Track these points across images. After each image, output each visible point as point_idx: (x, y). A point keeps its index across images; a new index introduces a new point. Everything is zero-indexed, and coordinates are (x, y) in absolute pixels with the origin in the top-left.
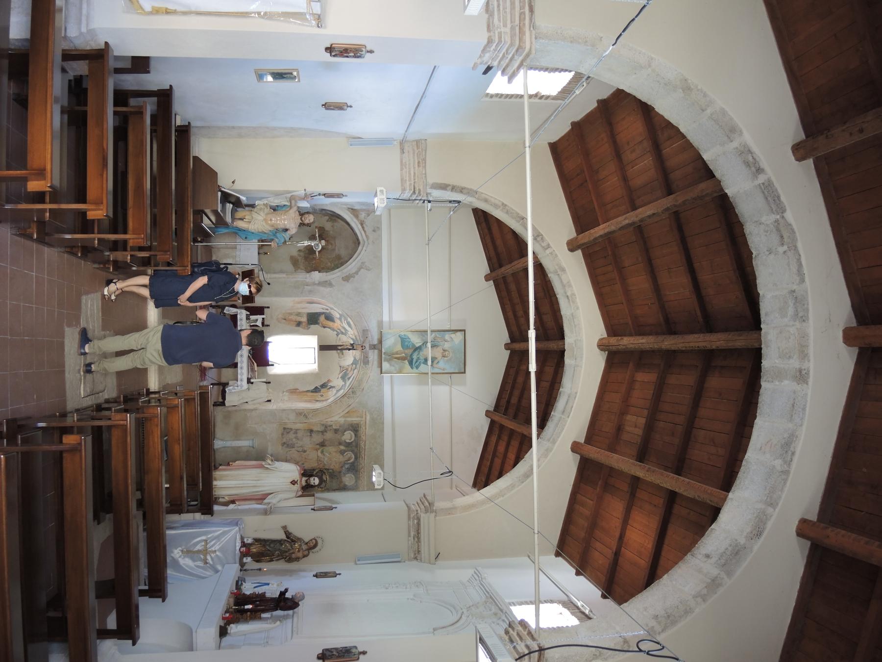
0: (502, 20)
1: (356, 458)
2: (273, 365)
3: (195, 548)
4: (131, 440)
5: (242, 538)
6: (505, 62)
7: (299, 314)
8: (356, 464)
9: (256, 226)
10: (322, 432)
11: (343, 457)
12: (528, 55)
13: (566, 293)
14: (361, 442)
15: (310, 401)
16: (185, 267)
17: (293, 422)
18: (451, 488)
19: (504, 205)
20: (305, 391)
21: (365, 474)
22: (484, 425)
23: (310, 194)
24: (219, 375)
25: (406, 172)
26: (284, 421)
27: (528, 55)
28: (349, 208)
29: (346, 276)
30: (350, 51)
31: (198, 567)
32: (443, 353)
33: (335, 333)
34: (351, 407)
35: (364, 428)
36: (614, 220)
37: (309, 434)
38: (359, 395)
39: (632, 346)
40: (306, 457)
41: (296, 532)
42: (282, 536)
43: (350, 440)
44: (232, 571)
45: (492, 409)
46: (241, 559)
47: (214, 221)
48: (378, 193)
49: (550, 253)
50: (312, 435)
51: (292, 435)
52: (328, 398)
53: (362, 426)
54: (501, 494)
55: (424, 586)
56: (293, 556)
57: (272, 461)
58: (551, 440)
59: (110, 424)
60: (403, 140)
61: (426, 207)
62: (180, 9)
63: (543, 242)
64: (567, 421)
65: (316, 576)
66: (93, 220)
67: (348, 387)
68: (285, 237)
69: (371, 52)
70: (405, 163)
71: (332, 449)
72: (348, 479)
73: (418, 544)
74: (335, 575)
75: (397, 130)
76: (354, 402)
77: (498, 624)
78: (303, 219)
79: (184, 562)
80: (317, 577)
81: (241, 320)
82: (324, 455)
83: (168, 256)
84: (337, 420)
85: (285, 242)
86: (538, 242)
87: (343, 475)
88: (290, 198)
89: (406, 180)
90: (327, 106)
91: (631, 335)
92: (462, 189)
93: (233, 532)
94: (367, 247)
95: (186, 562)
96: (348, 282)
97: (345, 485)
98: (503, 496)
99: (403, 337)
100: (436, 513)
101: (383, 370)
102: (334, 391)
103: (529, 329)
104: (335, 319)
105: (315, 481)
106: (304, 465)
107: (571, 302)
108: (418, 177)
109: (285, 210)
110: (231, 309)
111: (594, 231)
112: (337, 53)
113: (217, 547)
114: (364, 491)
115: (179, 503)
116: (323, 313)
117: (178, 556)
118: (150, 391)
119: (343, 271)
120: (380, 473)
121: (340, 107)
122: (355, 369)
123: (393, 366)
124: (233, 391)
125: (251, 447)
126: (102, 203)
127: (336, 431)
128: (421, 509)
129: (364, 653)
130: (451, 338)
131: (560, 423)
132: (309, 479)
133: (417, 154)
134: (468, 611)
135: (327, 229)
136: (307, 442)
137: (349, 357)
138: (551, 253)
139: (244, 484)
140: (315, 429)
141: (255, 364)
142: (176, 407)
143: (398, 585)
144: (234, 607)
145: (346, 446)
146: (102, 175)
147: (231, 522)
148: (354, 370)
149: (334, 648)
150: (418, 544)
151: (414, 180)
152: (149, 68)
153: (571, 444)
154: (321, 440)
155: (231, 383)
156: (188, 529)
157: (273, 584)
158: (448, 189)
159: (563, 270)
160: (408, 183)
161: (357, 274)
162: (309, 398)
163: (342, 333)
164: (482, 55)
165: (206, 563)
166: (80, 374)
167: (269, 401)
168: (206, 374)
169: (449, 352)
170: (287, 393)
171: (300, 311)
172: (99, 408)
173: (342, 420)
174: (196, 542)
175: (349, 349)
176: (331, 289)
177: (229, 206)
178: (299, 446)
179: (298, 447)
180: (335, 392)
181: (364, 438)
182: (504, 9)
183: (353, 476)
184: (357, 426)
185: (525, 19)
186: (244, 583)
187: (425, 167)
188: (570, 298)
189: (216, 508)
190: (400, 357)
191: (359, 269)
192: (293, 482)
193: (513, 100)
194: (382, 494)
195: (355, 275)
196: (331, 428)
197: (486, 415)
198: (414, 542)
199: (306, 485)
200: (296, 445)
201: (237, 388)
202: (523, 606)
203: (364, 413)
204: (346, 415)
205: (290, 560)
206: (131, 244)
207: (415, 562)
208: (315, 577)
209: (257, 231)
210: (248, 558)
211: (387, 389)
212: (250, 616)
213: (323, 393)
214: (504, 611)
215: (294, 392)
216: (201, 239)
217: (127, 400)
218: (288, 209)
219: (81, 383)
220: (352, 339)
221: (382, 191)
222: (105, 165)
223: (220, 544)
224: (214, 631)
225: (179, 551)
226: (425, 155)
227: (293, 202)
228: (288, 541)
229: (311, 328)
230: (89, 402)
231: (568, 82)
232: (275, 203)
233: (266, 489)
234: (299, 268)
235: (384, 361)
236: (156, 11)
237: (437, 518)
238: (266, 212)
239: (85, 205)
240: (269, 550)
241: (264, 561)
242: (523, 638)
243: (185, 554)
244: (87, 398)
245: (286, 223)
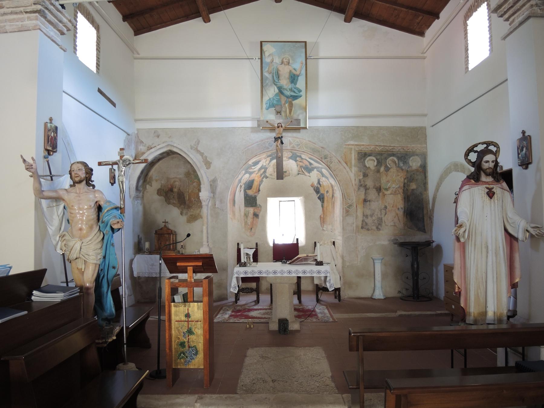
1: (393, 155)
2: (297, 240)
7: (246, 215)
8: (400, 156)
10: (366, 190)
11: (391, 168)
14: (377, 150)
15: (333, 204)
17: (356, 219)
18: (424, 58)
20: (323, 209)
21: (409, 145)
24: (308, 292)
25: (11, 25)
26: (355, 229)
29: (205, 165)
32: (284, 64)
33: (264, 179)
35: (362, 147)
38: (328, 151)
40: (392, 206)
43: (375, 161)
45: (343, 16)
50: (369, 199)
51: (369, 221)
52: (330, 185)
71: (384, 180)
72: (415, 163)
81: (246, 273)
84: (354, 175)
97: (421, 166)
99: (268, 105)
102: (323, 180)
104: (251, 179)
105: (491, 160)
106: (400, 208)
114: (427, 147)
125: (381, 261)
127: (365, 175)
130: (269, 55)
135: (159, 187)
139: (493, 271)
140: (363, 197)
145: (381, 166)
148: (302, 159)
154: (374, 191)
161: (203, 153)
162: (330, 204)
163: (265, 172)
167: (334, 243)
169: (283, 58)
170: (325, 226)
171: (243, 214)
173: (354, 169)
176: (219, 181)
179: (381, 214)
180: (324, 178)
183: (411, 158)
184: (361, 154)
190: (289, 108)
191: (198, 151)
192: (491, 195)
194: (433, 126)
196: (362, 180)
197: (349, 22)
200: (379, 216)
203: (347, 147)
204: (349, 164)
209: (99, 251)
211: (321, 123)
213: (324, 191)
220: (270, 162)
233: (501, 235)
234: (199, 214)
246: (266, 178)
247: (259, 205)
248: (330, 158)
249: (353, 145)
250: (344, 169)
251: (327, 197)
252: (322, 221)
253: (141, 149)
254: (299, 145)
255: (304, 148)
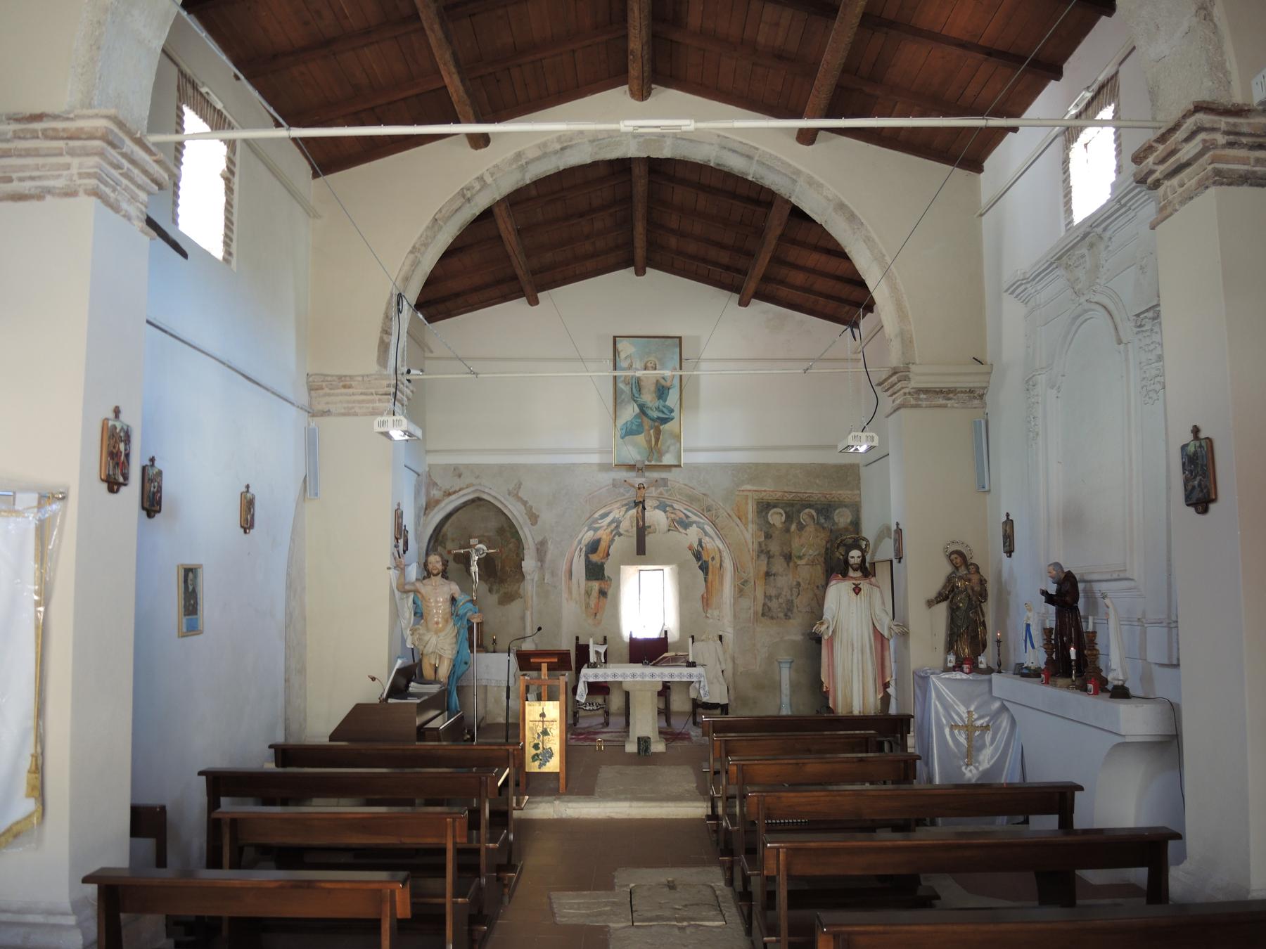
0: (56, 173)
1: (810, 506)
2: (666, 632)
3: (964, 745)
4: (814, 841)
5: (947, 670)
6: (138, 176)
7: (588, 594)
9: (447, 647)
11: (807, 525)
12: (121, 125)
13: (556, 152)
14: (785, 498)
15: (722, 577)
16: (509, 753)
19: (414, 250)
21: (834, 492)
22: (761, 310)
23: (395, 558)
26: (752, 614)
27: (121, 125)
28: (425, 514)
29: (530, 518)
30: (114, 447)
31: (992, 743)
34: (732, 513)
35: (764, 494)
36: (436, 54)
37: (772, 578)
39: (644, 32)
40: (807, 582)
41: (936, 584)
42: (942, 608)
44: (1003, 684)
45: (736, 297)
46: (982, 672)
47: (437, 712)
48: (383, 429)
49: (492, 177)
50: (773, 572)
51: (774, 604)
52: (716, 548)
53: (761, 496)
54: (879, 258)
55: (1034, 373)
56: (977, 588)
57: (822, 623)
58: (794, 177)
59: (785, 878)
60: (309, 412)
61: (418, 377)
62: (30, 748)
63: (473, 188)
64: (763, 151)
65: (1010, 552)
66: (413, 905)
67: (701, 518)
68: (463, 601)
69: (117, 412)
70: (345, 408)
71: (796, 543)
72: (842, 518)
73: (959, 392)
74: (1009, 523)
75: (292, 420)
76: (723, 509)
77: (1110, 238)
78: (435, 572)
79: (986, 761)
80: (1013, 551)
81: (596, 676)
82: (804, 555)
83: (489, 779)
85: (472, 601)
86: (473, 196)
87: (836, 527)
88: (401, 592)
89: (373, 408)
90: (247, 524)
91: (626, 37)
92: (387, 317)
93: (938, 683)
94: (484, 486)
95: (986, 759)
96: (538, 516)
97: (852, 523)
98: (884, 255)
99: (624, 431)
100: (909, 363)
101: (675, 463)
102: (706, 540)
103: (619, 130)
104: (595, 538)
106: (820, 586)
107: (569, 143)
108: (367, 388)
109: (422, 601)
110: (579, 691)
111: (455, 95)
112: (118, 472)
113: (962, 710)
115: (902, 765)
116: (587, 556)
117: (974, 771)
118: (710, 813)
119: (521, 522)
120: (854, 437)
121: (248, 505)
122: (672, 506)
123: (669, 447)
124: (707, 689)
125: (790, 665)
126: (380, 890)
127: (768, 536)
128: (903, 388)
129: (1196, 431)
131: (767, 163)
132: (851, 566)
133: (331, 389)
134: (1083, 294)
136: (784, 581)
137: (656, 517)
138: (492, 174)
139: (858, 669)
140: (764, 568)
141: (665, 655)
142: (741, 769)
143: (1032, 417)
144: (1073, 677)
145: (792, 522)
146: (330, 891)
147: (920, 687)
148: (675, 509)
149: (1185, 487)
150: (959, 392)
151: (372, 394)
152: (155, 808)
153: (801, 145)
154: (782, 560)
155: (693, 695)
156: (932, 756)
157: (1028, 618)
158: (387, 340)
159: (519, 155)
160: (378, 404)
163: (617, 527)
164: (123, 213)
165: (987, 727)
166: (686, 926)
167: (720, 638)
168: (678, 731)
169: (648, 362)
170: (709, 611)
171: (583, 592)
172: (744, 896)
173: (752, 527)
174: (954, 744)
175: (644, 508)
176: (549, 543)
177: (414, 687)
178: (789, 592)
179: (792, 595)
180: (707, 538)
181: (780, 494)
182: (38, 169)
183: (837, 511)
185: (54, 130)
186: (1025, 665)
187: (351, 377)
188: (565, 144)
189: (893, 710)
191: (520, 499)
193: (235, 219)
194: (867, 466)
195: (528, 505)
196: (763, 545)
197: (746, 306)
198: (954, 399)
199: (861, 571)
200: (789, 597)
201: (702, 684)
202: (1074, 207)
203: (741, 493)
204: (743, 520)
205: (983, 595)
206: (462, 840)
207: (987, 398)
208: (1013, 554)
209: (454, 646)
210: (979, 660)
211: (702, 458)
212: (1090, 650)
214: (1088, 230)
215: (707, 600)
216: (468, 733)
217: (728, 850)
218: (420, 596)
219: (701, 926)
220: (626, 512)
221: (381, 424)
222: (309, 884)
223: (957, 705)
224: (1123, 707)
225: (968, 769)
226: (332, 376)
227: (408, 587)
228: (952, 598)
229: (610, 575)
230: (732, 912)
231: (201, 120)
232: (410, 618)
233: (867, 633)
235: (661, 461)
236: (39, 790)
237: (917, 362)
238: (425, 632)
239: (383, 922)
240: (967, 627)
241: (985, 635)
242: (1173, 147)
243: (973, 760)
244: (727, 914)
245: (441, 600)
246: (619, 536)
247: (608, 577)
248: (716, 510)
249: (750, 491)
250: (737, 527)
251: (713, 566)
252: (705, 604)
253: (434, 495)
254: (670, 490)
255: (677, 494)
